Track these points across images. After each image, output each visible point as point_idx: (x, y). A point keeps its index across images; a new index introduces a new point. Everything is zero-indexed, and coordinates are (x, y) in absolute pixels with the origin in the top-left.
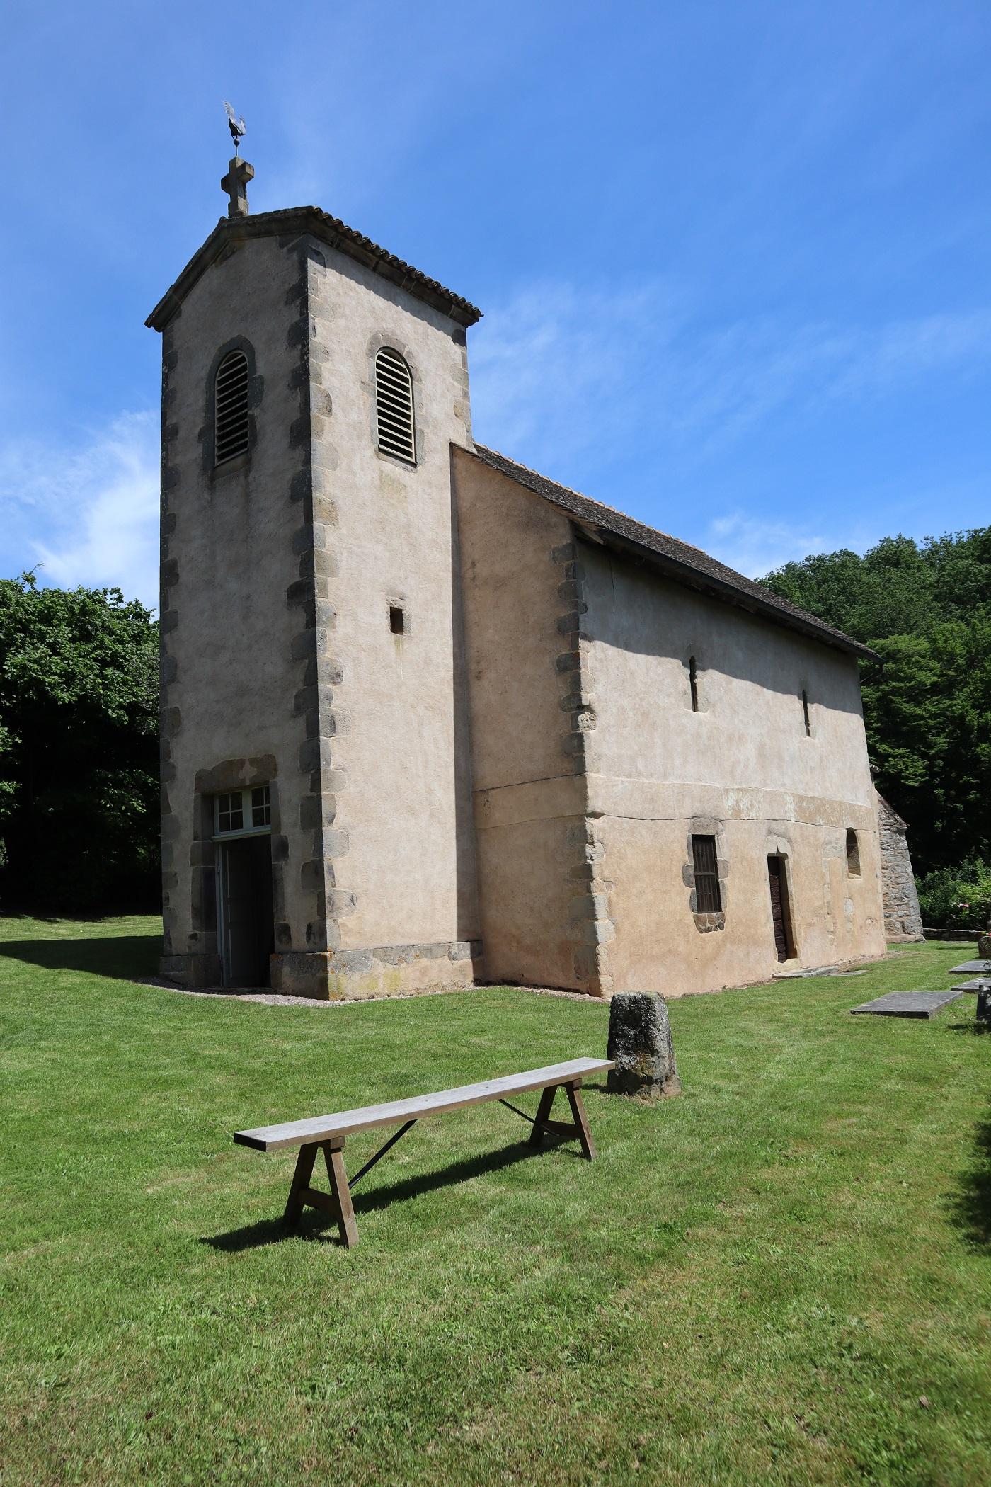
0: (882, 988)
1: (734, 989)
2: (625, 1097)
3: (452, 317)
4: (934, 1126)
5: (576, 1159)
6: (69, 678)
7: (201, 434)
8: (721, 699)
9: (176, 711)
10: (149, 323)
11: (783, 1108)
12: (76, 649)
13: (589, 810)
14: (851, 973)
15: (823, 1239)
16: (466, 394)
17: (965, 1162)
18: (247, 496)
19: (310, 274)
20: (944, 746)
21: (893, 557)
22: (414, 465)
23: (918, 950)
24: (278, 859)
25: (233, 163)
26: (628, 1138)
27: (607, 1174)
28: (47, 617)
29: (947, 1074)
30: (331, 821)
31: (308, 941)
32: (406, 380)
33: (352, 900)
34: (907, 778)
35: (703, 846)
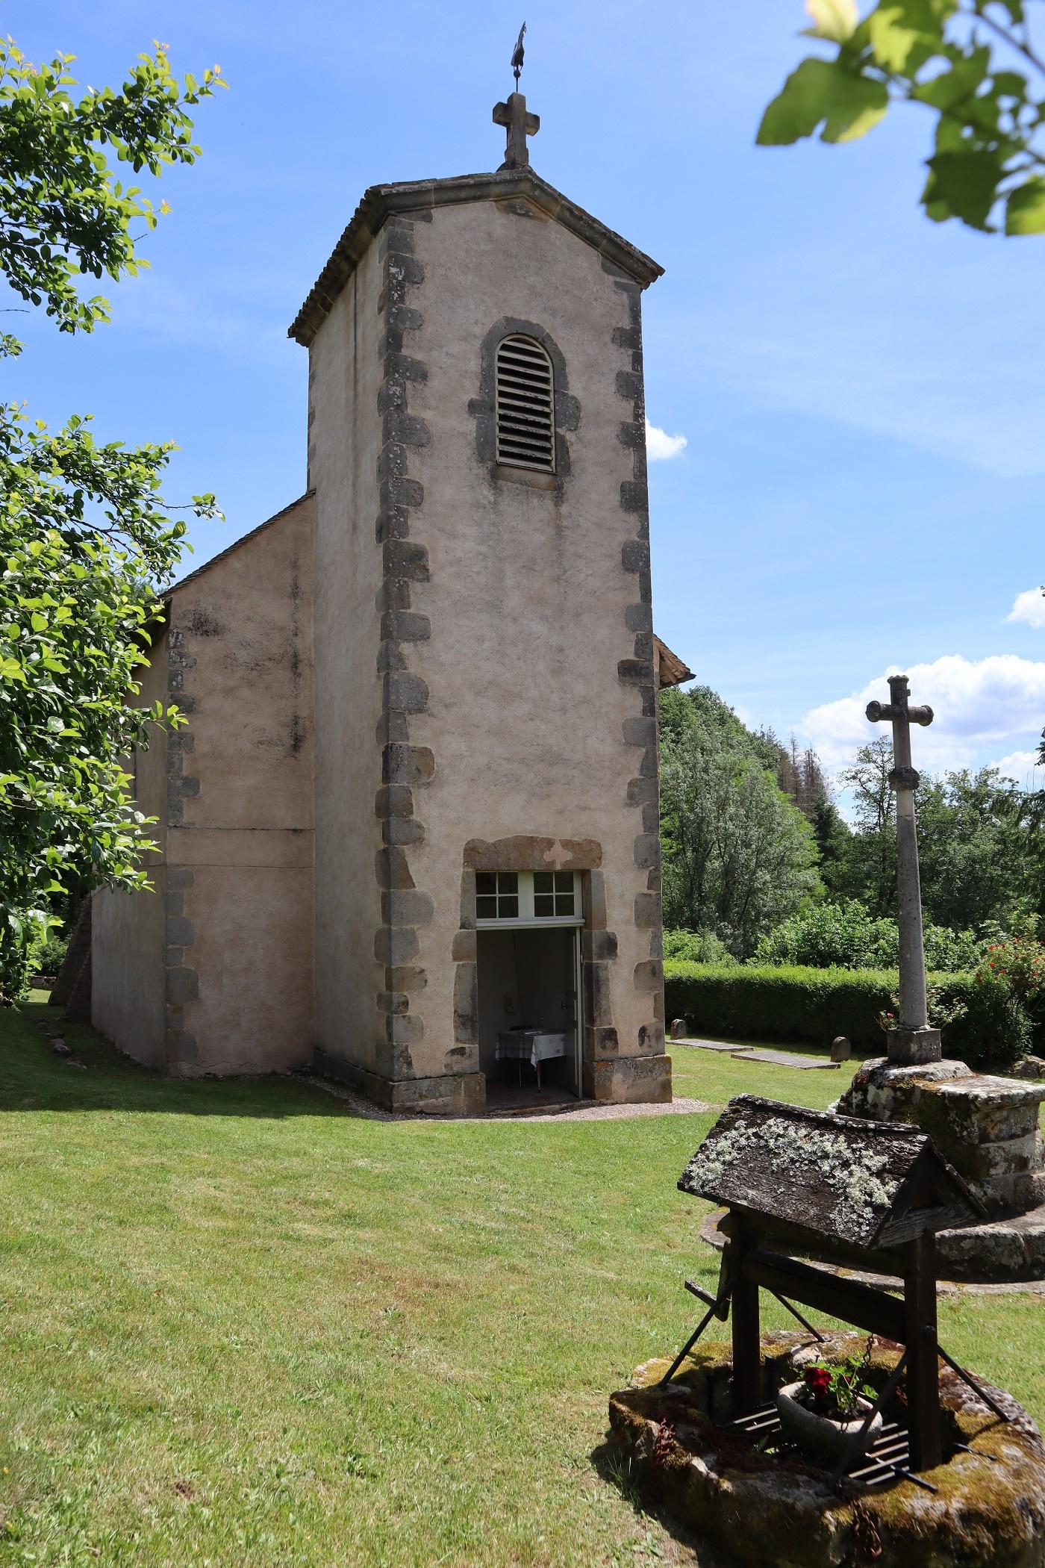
24: (601, 957)
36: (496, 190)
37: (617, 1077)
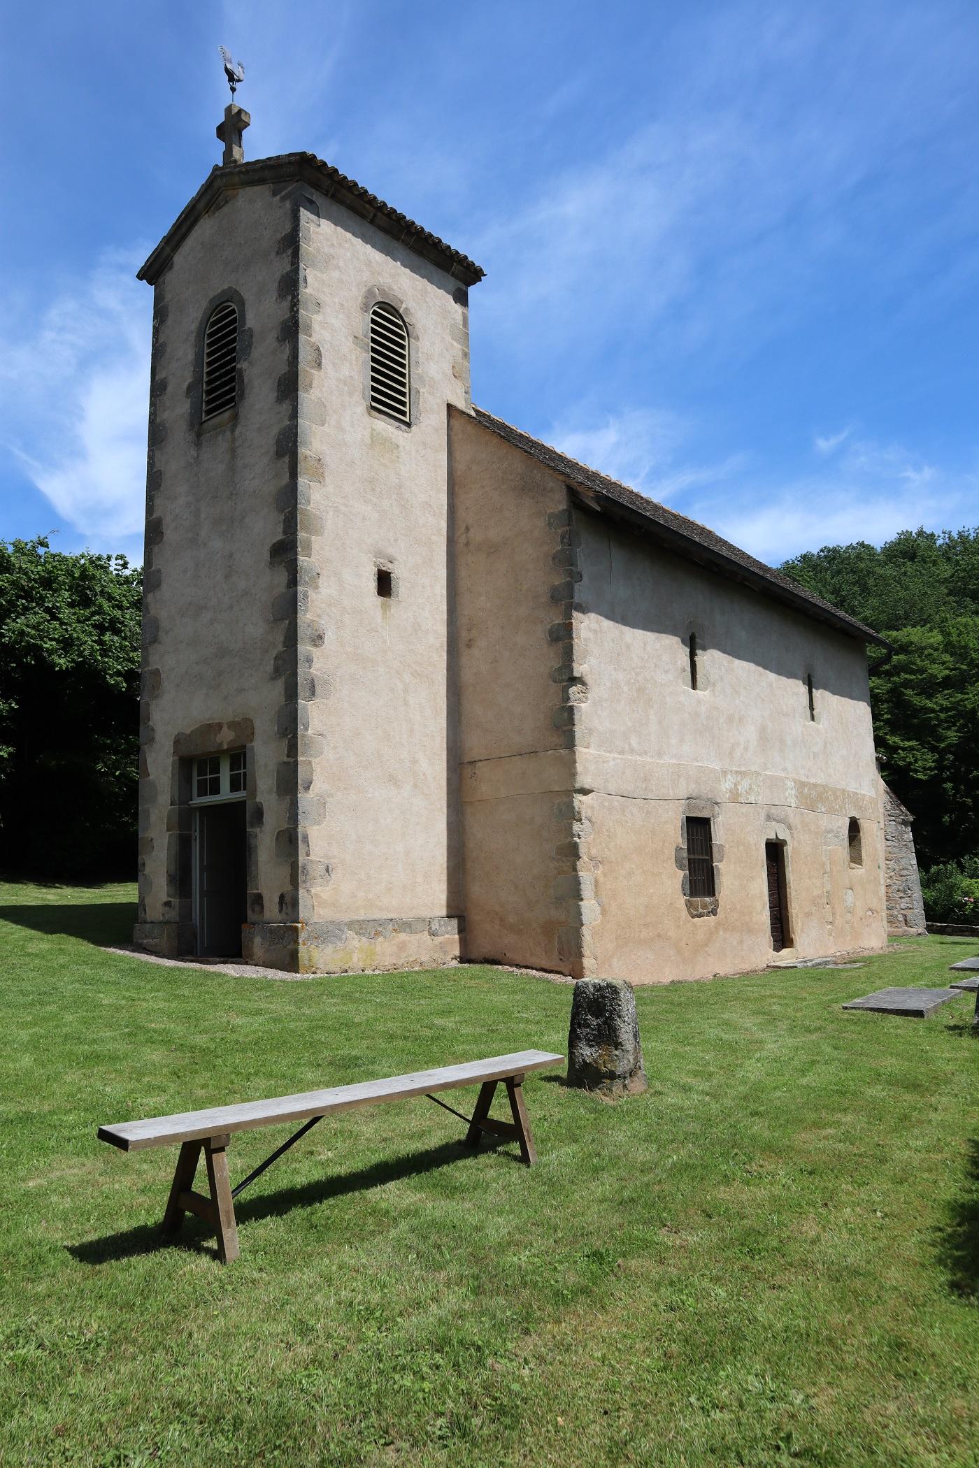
0: (878, 983)
1: (726, 978)
2: (584, 1092)
3: (453, 275)
4: (919, 1143)
5: (514, 1164)
6: (67, 644)
7: (189, 389)
8: (721, 679)
9: (157, 673)
10: (142, 276)
11: (755, 1114)
12: (74, 614)
13: (577, 786)
14: (849, 966)
15: (777, 1281)
16: (466, 355)
17: (952, 1187)
18: (233, 452)
19: (302, 222)
20: (954, 740)
21: (908, 550)
22: (409, 425)
23: (919, 945)
24: (252, 826)
25: (229, 110)
26: (576, 1141)
27: (544, 1184)
28: (48, 582)
29: (940, 1081)
30: (307, 788)
31: (280, 911)
32: (402, 338)
33: (327, 871)
34: (916, 771)
35: (698, 829)
36: (201, 206)
37: (258, 940)
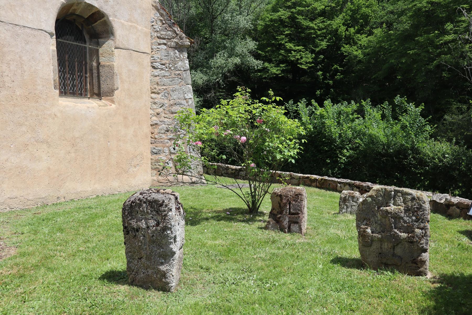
34: (301, 64)
